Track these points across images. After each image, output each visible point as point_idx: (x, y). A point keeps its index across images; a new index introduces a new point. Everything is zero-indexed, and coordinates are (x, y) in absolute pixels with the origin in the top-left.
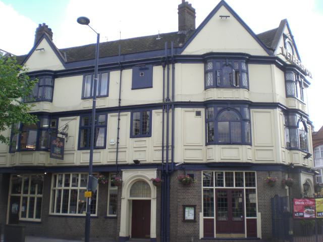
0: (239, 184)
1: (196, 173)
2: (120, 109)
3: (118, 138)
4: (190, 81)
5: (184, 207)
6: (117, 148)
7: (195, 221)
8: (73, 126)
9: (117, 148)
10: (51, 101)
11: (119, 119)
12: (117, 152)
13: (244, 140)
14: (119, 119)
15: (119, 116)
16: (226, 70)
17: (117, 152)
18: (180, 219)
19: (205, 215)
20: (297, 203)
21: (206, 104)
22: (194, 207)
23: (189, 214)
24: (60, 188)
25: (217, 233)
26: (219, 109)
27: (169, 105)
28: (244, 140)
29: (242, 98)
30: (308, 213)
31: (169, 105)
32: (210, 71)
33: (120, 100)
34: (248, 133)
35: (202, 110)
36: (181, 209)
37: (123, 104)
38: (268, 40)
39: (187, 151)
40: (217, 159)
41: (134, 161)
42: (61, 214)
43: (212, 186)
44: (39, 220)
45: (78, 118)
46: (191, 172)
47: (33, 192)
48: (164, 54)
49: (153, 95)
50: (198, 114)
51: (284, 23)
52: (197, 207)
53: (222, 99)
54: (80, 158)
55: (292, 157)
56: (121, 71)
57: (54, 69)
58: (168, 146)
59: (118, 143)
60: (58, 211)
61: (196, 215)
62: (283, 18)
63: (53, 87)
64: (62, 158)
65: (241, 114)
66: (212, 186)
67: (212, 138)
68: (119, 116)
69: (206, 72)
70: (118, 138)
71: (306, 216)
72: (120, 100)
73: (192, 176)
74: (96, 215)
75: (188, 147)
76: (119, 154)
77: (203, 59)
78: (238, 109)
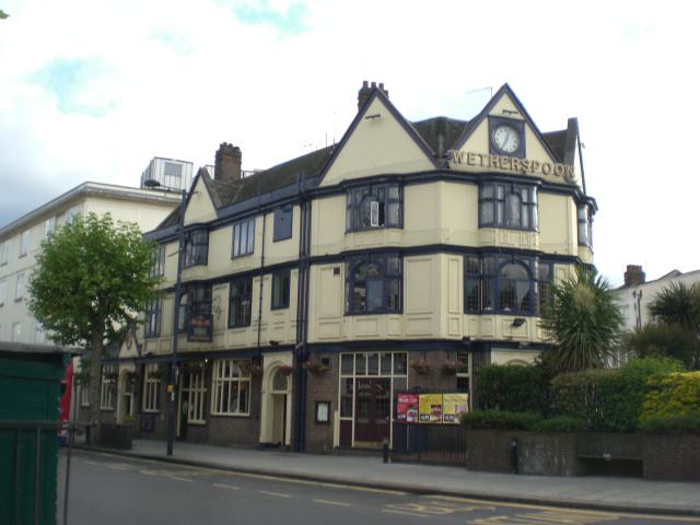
0: (386, 370)
1: (332, 357)
2: (262, 271)
3: (260, 312)
4: (329, 224)
5: (317, 403)
6: (260, 325)
7: (329, 423)
8: (222, 295)
9: (260, 325)
10: (401, 226)
11: (262, 285)
12: (259, 330)
13: (393, 304)
14: (262, 285)
15: (262, 281)
16: (514, 200)
17: (259, 330)
18: (313, 420)
19: (342, 415)
20: (400, 400)
21: (343, 257)
22: (328, 403)
23: (322, 414)
24: (227, 379)
25: (355, 439)
26: (501, 260)
27: (305, 262)
28: (393, 304)
29: (386, 244)
30: (411, 414)
31: (305, 262)
32: (488, 200)
33: (263, 258)
34: (396, 297)
35: (342, 266)
36: (313, 407)
37: (268, 263)
38: (562, 144)
39: (324, 327)
40: (351, 337)
41: (271, 342)
42: (221, 413)
43: (357, 374)
44: (203, 422)
45: (228, 285)
46: (326, 356)
47: (199, 387)
48: (294, 190)
49: (288, 251)
50: (337, 271)
51: (573, 123)
52: (332, 404)
53: (361, 248)
54: (231, 339)
55: (480, 326)
56: (265, 216)
57: (205, 220)
58: (302, 323)
59: (260, 318)
60: (225, 410)
61: (330, 414)
62: (571, 117)
63: (401, 202)
64: (211, 341)
65: (382, 268)
66: (357, 374)
67: (356, 306)
68: (262, 281)
69: (481, 201)
70: (260, 312)
71: (409, 419)
72: (263, 258)
73: (326, 361)
74: (248, 415)
75: (326, 321)
76: (262, 333)
77: (479, 180)
78: (527, 262)
